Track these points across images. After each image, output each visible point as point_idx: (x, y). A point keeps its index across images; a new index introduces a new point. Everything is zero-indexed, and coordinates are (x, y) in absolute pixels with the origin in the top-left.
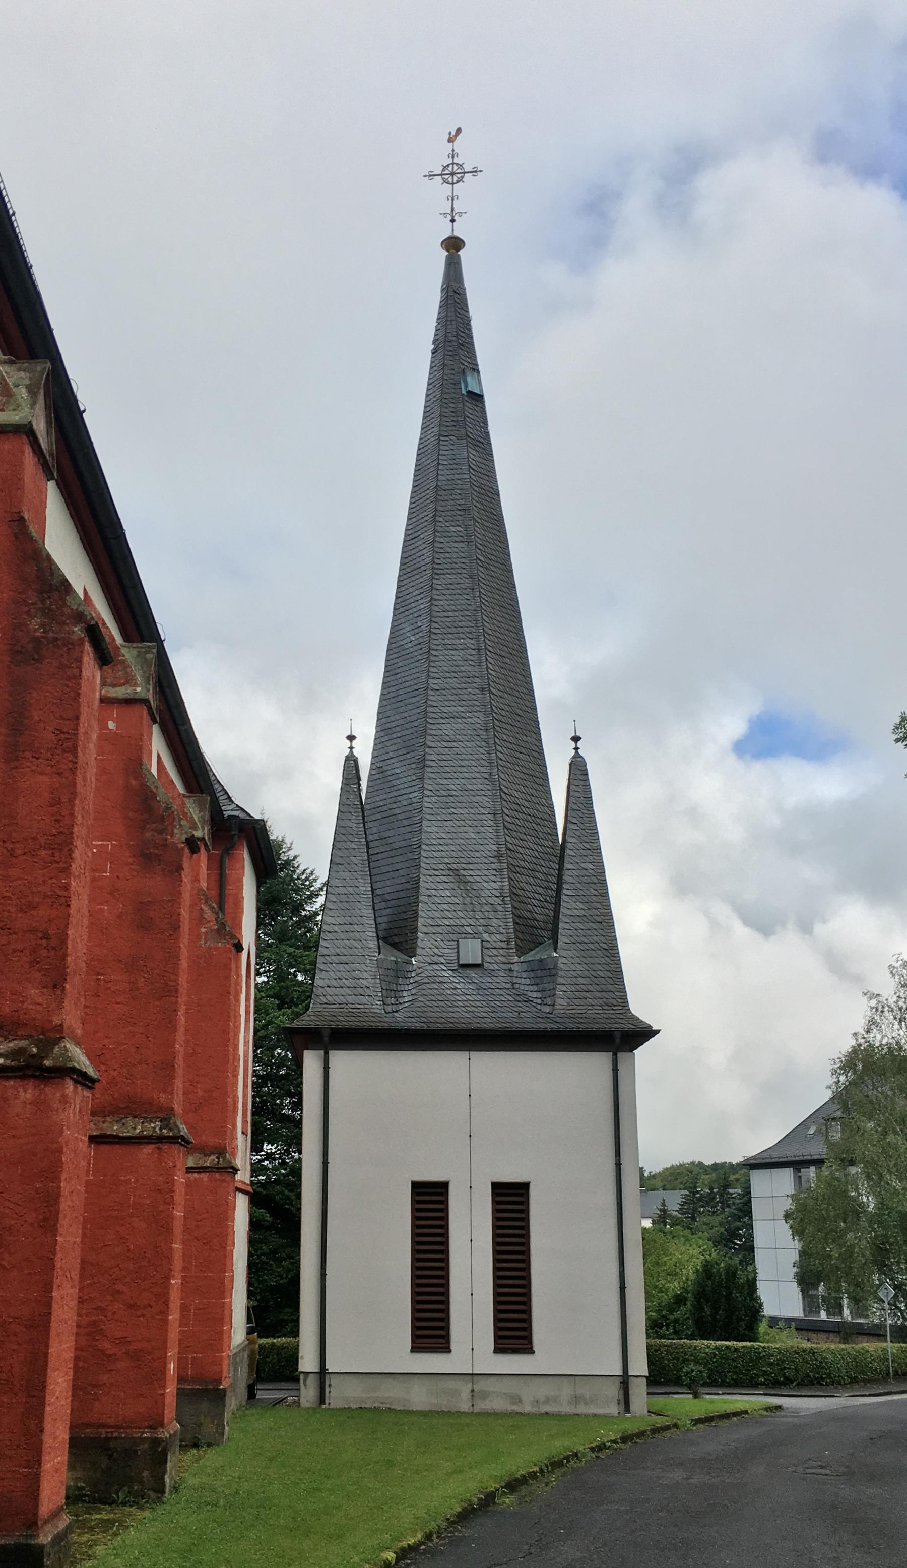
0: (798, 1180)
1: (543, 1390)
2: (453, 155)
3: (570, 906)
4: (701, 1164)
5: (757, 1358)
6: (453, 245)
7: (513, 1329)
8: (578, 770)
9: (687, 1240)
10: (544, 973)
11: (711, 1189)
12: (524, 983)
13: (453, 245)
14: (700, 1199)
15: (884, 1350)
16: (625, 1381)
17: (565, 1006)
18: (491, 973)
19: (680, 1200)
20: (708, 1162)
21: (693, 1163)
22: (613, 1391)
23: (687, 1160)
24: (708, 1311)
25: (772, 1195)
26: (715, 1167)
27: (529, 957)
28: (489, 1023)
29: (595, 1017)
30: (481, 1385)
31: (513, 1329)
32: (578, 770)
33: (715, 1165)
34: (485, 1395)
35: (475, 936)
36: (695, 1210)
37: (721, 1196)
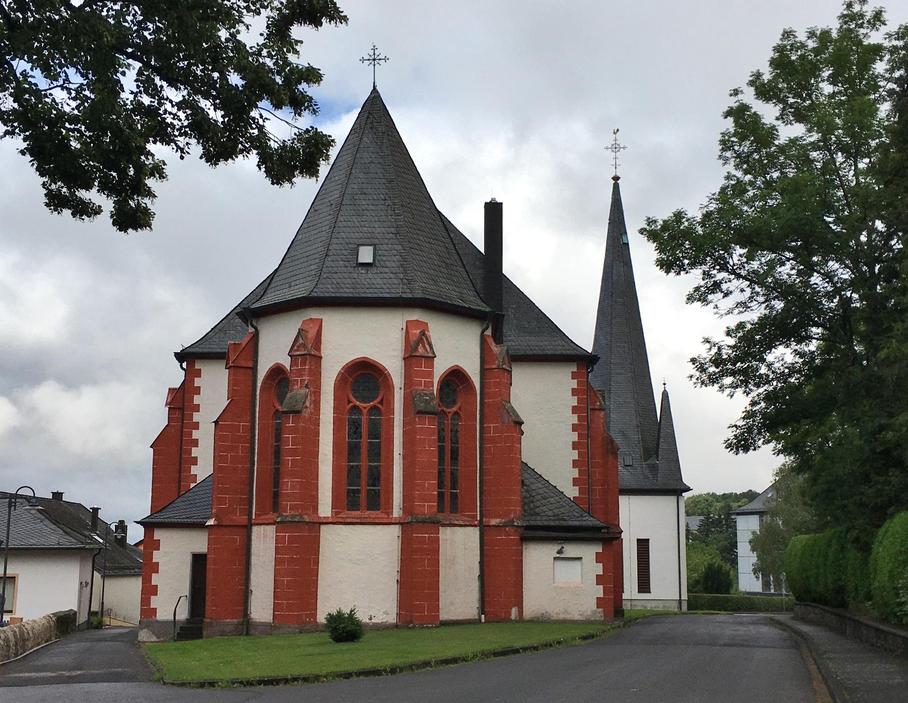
0: (761, 520)
1: (654, 604)
2: (616, 140)
3: (663, 446)
4: (714, 495)
5: (727, 600)
6: (616, 178)
7: (644, 585)
8: (665, 395)
9: (703, 550)
10: (654, 469)
11: (720, 516)
12: (647, 472)
13: (616, 178)
14: (712, 523)
15: (782, 600)
16: (680, 601)
17: (660, 483)
18: (636, 468)
19: (698, 523)
20: (719, 493)
21: (708, 494)
22: (676, 604)
23: (704, 492)
24: (709, 583)
25: (747, 527)
26: (725, 496)
27: (648, 462)
28: (635, 487)
29: (672, 485)
30: (634, 603)
31: (644, 585)
32: (665, 395)
33: (724, 494)
34: (635, 606)
35: (630, 455)
36: (708, 530)
37: (726, 521)
